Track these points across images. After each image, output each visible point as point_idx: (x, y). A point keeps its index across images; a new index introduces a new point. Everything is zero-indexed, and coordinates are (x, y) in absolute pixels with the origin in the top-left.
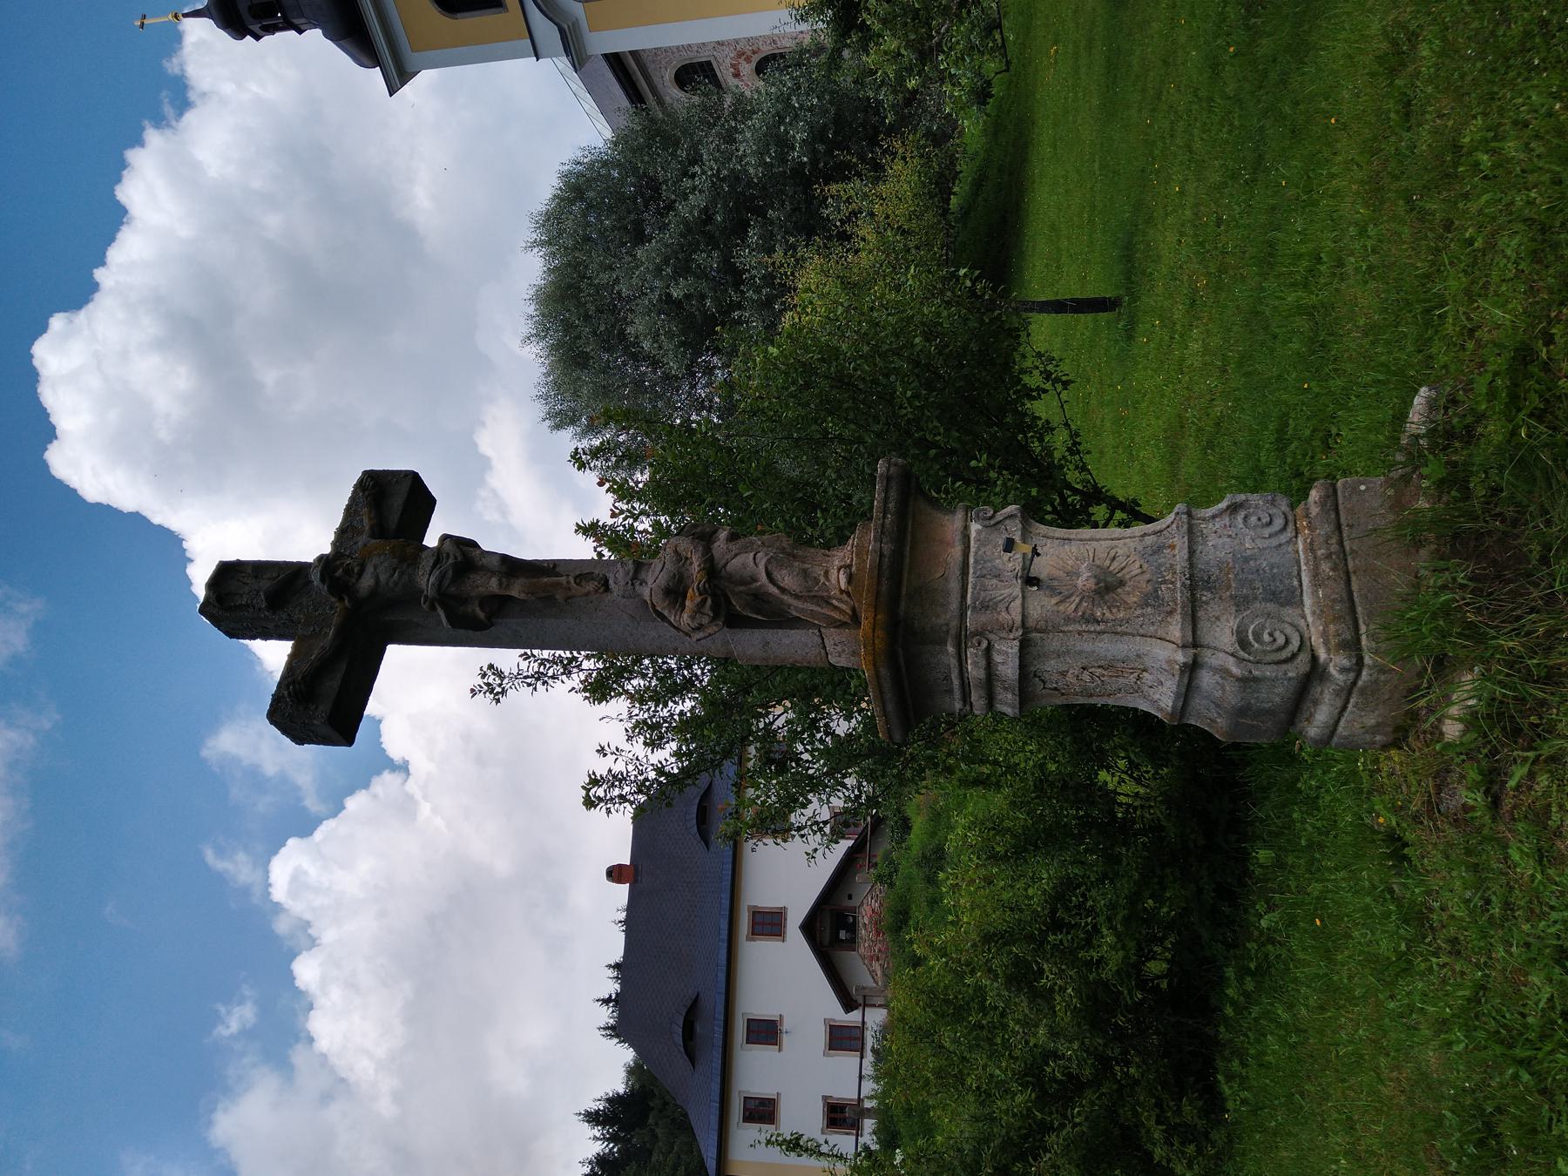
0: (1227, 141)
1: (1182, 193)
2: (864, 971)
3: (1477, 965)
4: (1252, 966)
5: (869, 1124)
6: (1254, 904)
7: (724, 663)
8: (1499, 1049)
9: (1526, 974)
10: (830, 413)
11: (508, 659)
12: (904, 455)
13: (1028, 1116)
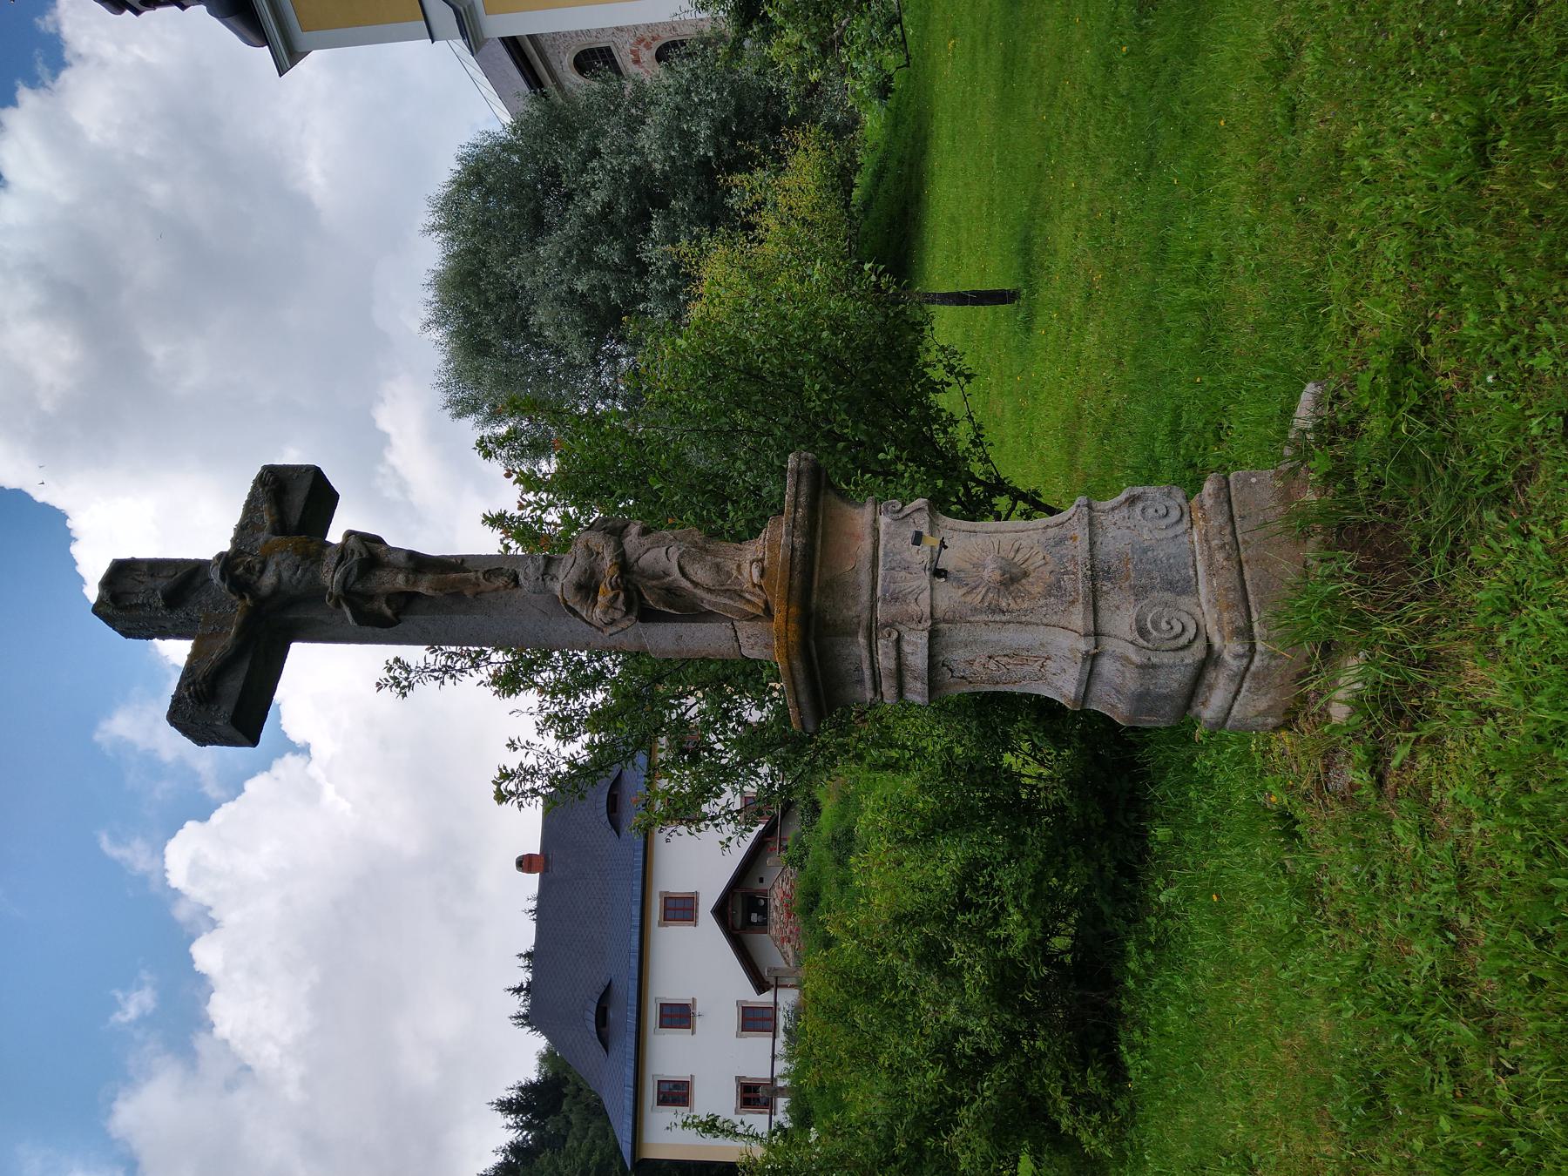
0: (1120, 139)
1: (1077, 188)
2: (774, 951)
3: (1365, 937)
4: (1152, 939)
5: (782, 1103)
6: (1153, 879)
7: (635, 657)
8: (1385, 1016)
9: (1410, 944)
10: (739, 406)
11: (415, 654)
12: (812, 449)
13: (939, 1092)
